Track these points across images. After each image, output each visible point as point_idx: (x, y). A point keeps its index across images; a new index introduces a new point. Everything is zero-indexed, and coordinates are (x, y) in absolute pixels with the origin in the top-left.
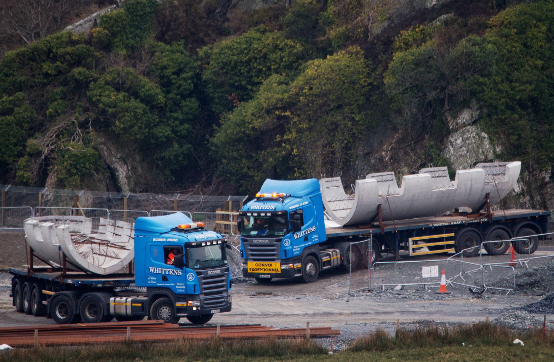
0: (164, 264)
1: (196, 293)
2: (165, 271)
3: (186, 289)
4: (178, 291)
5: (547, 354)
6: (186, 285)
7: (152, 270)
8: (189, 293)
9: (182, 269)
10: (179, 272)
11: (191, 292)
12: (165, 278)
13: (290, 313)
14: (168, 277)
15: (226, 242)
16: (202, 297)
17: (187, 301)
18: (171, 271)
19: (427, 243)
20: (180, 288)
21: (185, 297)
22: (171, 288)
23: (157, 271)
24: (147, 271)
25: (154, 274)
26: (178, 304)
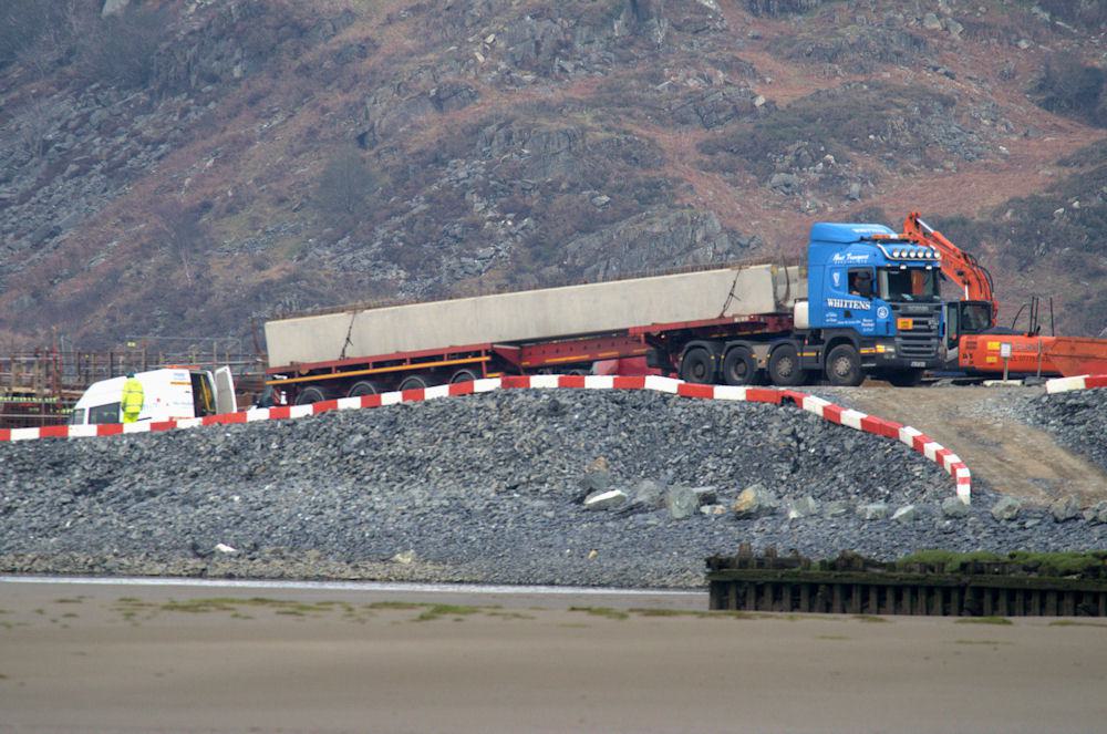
0: (847, 294)
1: (890, 335)
2: (848, 304)
3: (875, 327)
4: (864, 330)
5: (714, 39)
6: (875, 321)
7: (830, 304)
8: (880, 333)
9: (871, 300)
10: (866, 305)
11: (883, 333)
12: (848, 314)
13: (382, 600)
14: (853, 313)
15: (939, 269)
16: (898, 340)
17: (874, 345)
18: (857, 303)
19: (885, 599)
20: (867, 326)
21: (872, 340)
22: (857, 328)
23: (838, 304)
24: (824, 305)
25: (834, 309)
26: (864, 351)
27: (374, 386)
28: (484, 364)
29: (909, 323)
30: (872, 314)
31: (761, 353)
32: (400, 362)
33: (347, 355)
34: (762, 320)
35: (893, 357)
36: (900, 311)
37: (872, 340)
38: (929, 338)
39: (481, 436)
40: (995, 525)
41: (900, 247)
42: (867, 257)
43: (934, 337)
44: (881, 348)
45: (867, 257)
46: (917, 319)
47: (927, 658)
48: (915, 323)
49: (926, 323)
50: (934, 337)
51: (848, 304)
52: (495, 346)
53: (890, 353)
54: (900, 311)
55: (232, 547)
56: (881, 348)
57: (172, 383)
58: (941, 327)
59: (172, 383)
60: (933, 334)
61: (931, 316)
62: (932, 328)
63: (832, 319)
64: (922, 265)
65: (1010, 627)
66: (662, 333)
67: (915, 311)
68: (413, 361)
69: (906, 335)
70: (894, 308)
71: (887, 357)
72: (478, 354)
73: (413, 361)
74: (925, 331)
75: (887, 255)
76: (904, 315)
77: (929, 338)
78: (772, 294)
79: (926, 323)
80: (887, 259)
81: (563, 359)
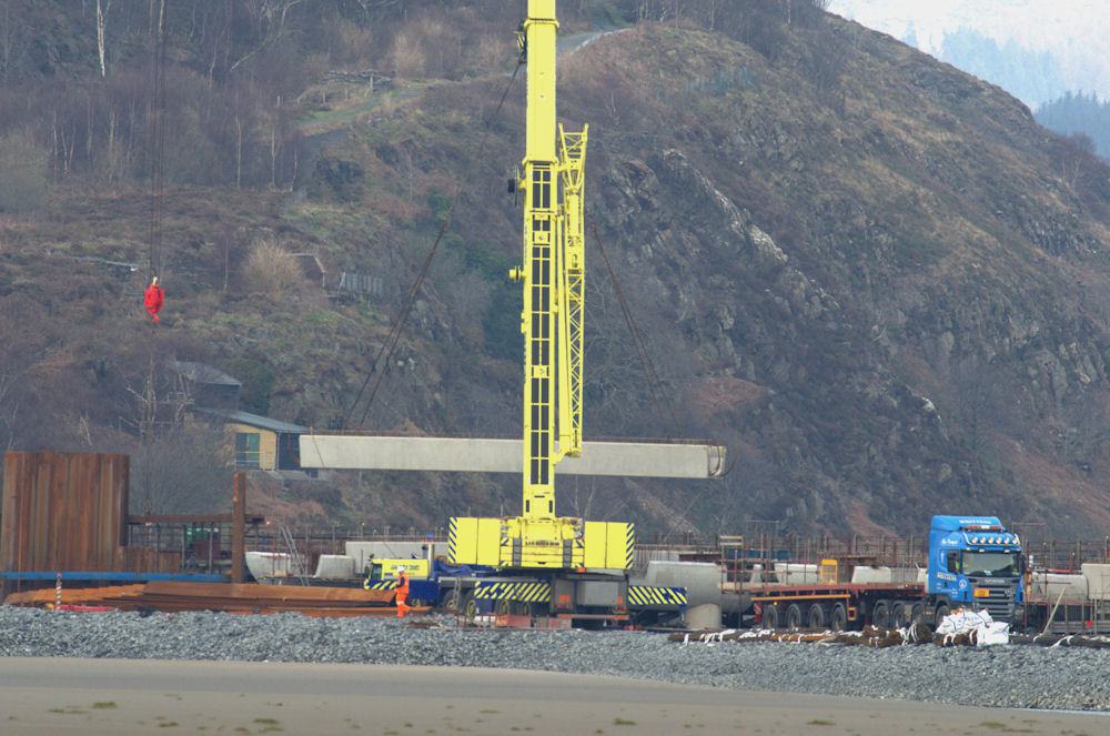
29: (986, 593)
30: (956, 585)
33: (808, 581)
38: (1006, 604)
39: (158, 636)
40: (893, 90)
41: (988, 535)
46: (991, 607)
48: (991, 592)
49: (1003, 592)
58: (1018, 595)
61: (1008, 587)
63: (940, 588)
64: (1001, 549)
66: (866, 591)
68: (818, 593)
73: (818, 593)
76: (980, 587)
77: (1006, 604)
78: (706, 467)
79: (1003, 592)
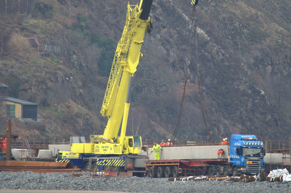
1: (244, 165)
2: (233, 157)
4: (237, 164)
20: (238, 163)
21: (239, 167)
26: (239, 170)
27: (161, 168)
28: (178, 166)
29: (251, 162)
30: (240, 160)
31: (222, 168)
32: (165, 163)
34: (225, 161)
35: (245, 171)
36: (248, 159)
37: (239, 167)
38: (258, 167)
42: (240, 144)
43: (260, 166)
44: (242, 169)
45: (240, 144)
46: (253, 161)
47: (68, 107)
48: (252, 162)
50: (260, 166)
51: (233, 157)
52: (181, 161)
53: (244, 171)
54: (248, 159)
55: (207, 33)
56: (242, 169)
57: (55, 148)
59: (55, 148)
60: (260, 165)
61: (259, 160)
62: (259, 164)
65: (105, 144)
67: (253, 159)
68: (168, 163)
69: (250, 165)
70: (246, 158)
71: (243, 171)
72: (177, 163)
73: (168, 163)
74: (257, 165)
75: (244, 144)
76: (249, 160)
77: (258, 167)
79: (257, 162)
80: (244, 145)
81: (196, 165)
